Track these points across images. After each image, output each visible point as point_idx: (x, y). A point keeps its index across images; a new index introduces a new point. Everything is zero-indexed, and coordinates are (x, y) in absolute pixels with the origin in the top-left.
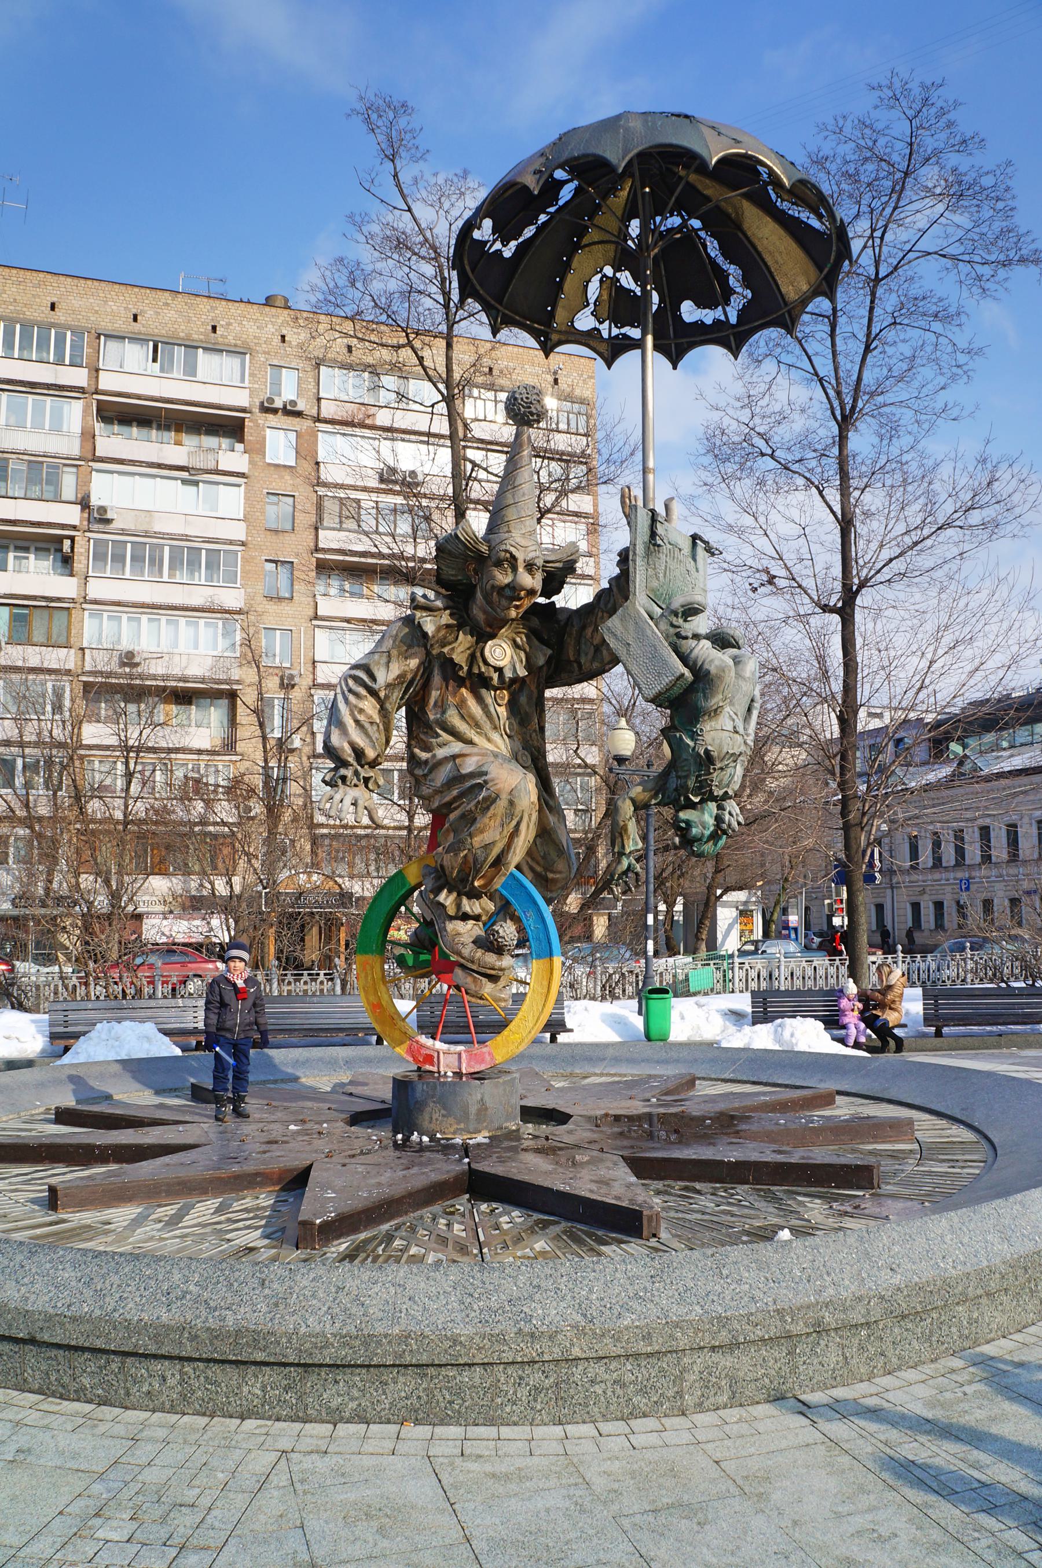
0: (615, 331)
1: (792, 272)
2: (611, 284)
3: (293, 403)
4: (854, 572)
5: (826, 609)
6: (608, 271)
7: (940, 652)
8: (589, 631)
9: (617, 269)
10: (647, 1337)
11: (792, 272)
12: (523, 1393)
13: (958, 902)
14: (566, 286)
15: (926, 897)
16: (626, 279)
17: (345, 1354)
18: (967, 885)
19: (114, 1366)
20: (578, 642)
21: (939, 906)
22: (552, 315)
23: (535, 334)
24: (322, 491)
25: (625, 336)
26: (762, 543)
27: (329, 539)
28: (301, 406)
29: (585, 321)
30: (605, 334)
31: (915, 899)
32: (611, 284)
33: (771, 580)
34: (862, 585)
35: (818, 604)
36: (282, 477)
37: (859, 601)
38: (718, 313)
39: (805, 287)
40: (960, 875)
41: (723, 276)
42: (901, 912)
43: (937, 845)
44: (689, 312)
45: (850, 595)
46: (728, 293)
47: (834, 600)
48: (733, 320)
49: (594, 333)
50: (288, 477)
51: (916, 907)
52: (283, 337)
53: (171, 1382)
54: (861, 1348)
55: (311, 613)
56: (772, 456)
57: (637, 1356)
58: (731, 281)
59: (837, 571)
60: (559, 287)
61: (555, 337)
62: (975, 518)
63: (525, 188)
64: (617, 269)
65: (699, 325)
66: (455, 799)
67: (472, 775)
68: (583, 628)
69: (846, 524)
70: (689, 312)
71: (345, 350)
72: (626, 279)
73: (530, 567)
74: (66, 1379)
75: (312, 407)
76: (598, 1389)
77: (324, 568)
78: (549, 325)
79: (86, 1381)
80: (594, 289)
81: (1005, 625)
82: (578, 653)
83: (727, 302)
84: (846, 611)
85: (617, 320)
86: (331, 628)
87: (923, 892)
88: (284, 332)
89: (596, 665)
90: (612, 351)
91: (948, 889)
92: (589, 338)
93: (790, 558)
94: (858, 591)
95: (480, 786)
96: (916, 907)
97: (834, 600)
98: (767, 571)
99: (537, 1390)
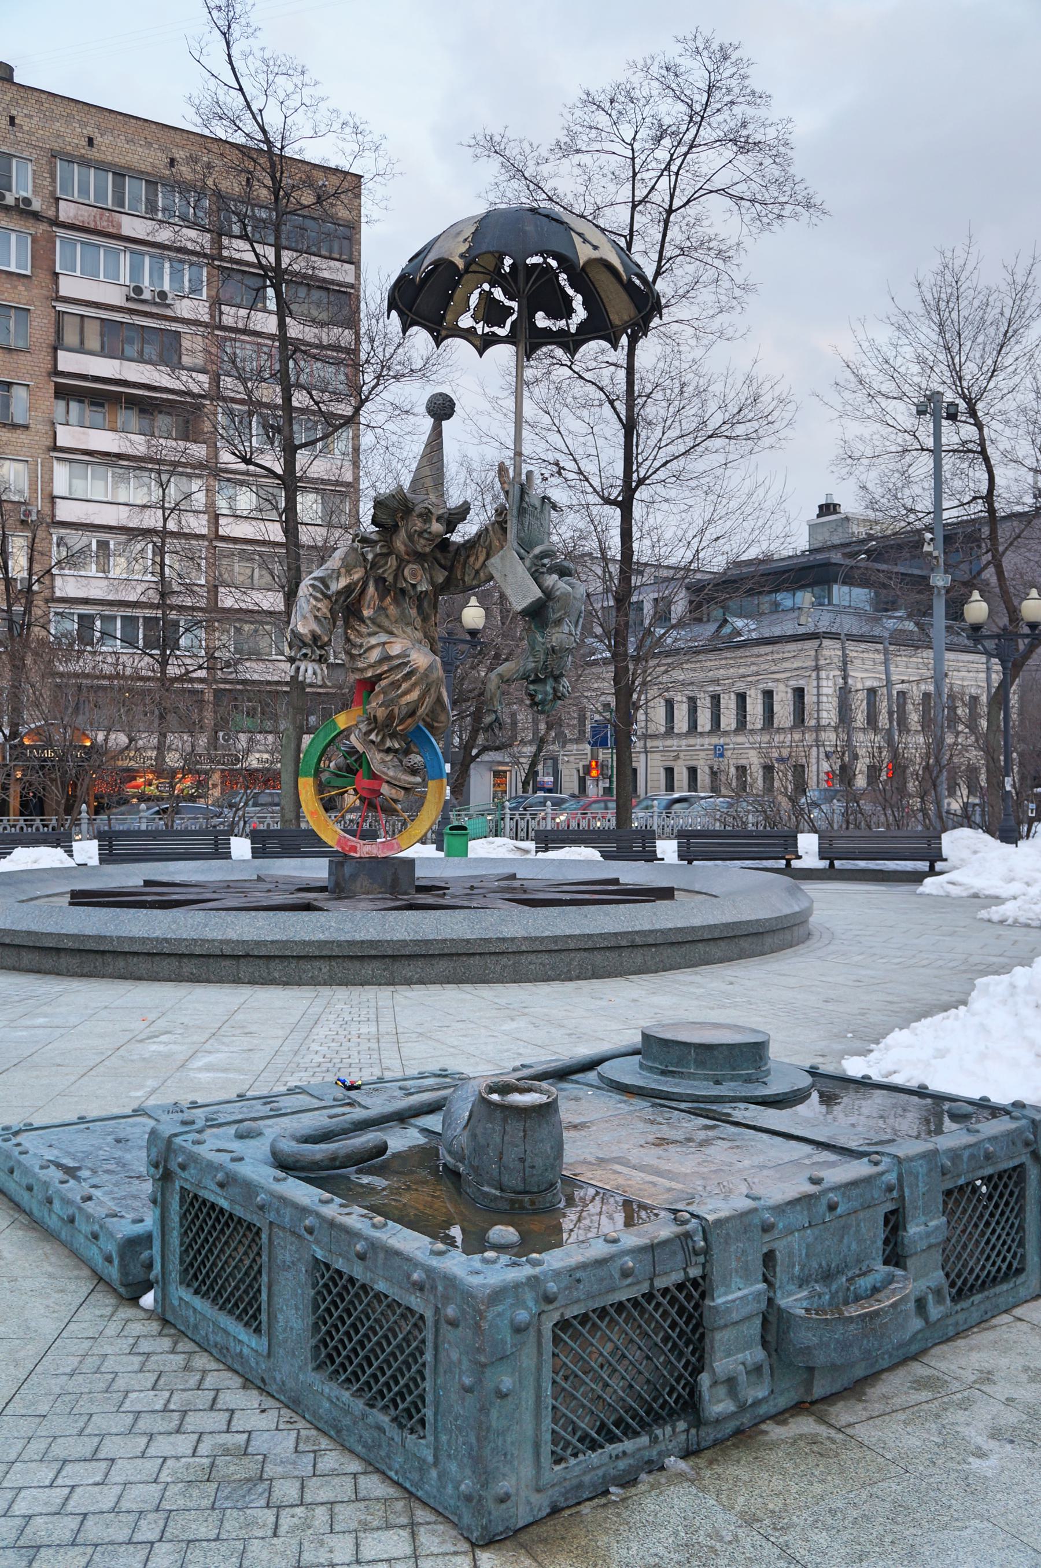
0: (487, 330)
1: (620, 309)
2: (486, 297)
3: (27, 201)
4: (634, 468)
5: (608, 501)
6: (486, 287)
7: (704, 544)
8: (472, 559)
9: (492, 286)
10: (556, 942)
11: (620, 309)
12: (498, 968)
13: (711, 768)
14: (456, 297)
15: (680, 762)
16: (498, 293)
17: (417, 950)
18: (719, 752)
19: (293, 966)
20: (464, 567)
21: (693, 771)
22: (443, 317)
23: (431, 331)
24: (61, 307)
25: (494, 334)
26: (555, 438)
27: (68, 362)
28: (37, 205)
29: (466, 321)
30: (480, 332)
31: (669, 764)
32: (486, 297)
33: (560, 470)
34: (641, 482)
35: (602, 498)
36: (15, 287)
37: (637, 495)
38: (562, 323)
39: (626, 318)
40: (715, 740)
41: (569, 300)
42: (655, 777)
43: (693, 710)
44: (542, 321)
45: (629, 491)
46: (569, 312)
47: (615, 493)
48: (573, 330)
49: (472, 331)
50: (21, 288)
51: (670, 771)
52: (12, 119)
53: (324, 970)
54: (653, 958)
55: (49, 442)
56: (570, 367)
57: (550, 951)
58: (574, 304)
59: (619, 469)
60: (451, 298)
61: (444, 333)
62: (740, 430)
63: (453, 264)
64: (492, 286)
65: (546, 331)
66: (385, 672)
67: (398, 657)
68: (468, 557)
69: (630, 427)
70: (542, 321)
71: (84, 142)
72: (498, 293)
73: (439, 519)
74: (265, 975)
75: (48, 208)
76: (533, 967)
77: (63, 393)
78: (441, 325)
79: (276, 975)
80: (474, 299)
81: (760, 523)
82: (464, 574)
83: (569, 317)
84: (626, 506)
85: (489, 322)
86: (70, 461)
87: (677, 758)
88: (14, 112)
89: (474, 583)
90: (484, 344)
91: (702, 754)
92: (468, 334)
93: (579, 453)
94: (637, 487)
95: (406, 664)
96: (670, 771)
97: (615, 493)
98: (557, 464)
99: (505, 967)
